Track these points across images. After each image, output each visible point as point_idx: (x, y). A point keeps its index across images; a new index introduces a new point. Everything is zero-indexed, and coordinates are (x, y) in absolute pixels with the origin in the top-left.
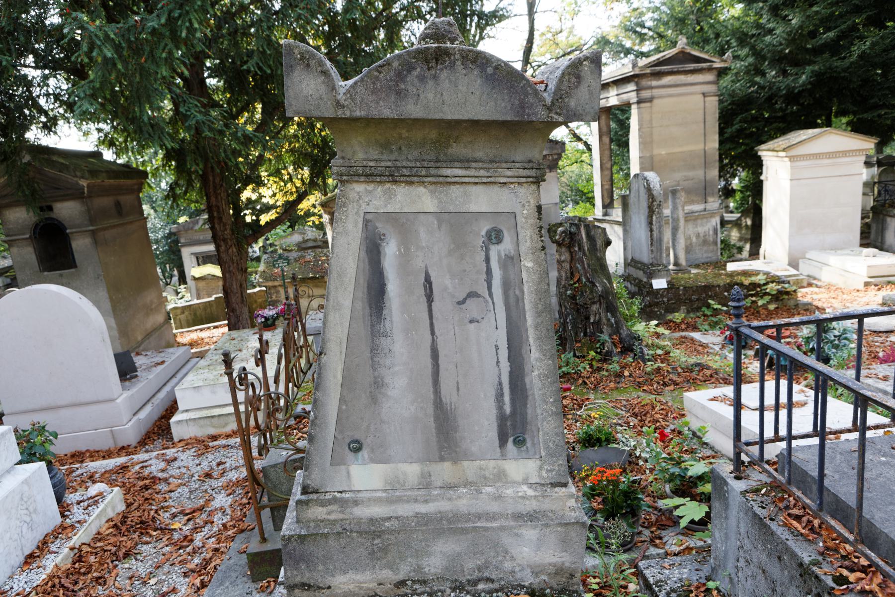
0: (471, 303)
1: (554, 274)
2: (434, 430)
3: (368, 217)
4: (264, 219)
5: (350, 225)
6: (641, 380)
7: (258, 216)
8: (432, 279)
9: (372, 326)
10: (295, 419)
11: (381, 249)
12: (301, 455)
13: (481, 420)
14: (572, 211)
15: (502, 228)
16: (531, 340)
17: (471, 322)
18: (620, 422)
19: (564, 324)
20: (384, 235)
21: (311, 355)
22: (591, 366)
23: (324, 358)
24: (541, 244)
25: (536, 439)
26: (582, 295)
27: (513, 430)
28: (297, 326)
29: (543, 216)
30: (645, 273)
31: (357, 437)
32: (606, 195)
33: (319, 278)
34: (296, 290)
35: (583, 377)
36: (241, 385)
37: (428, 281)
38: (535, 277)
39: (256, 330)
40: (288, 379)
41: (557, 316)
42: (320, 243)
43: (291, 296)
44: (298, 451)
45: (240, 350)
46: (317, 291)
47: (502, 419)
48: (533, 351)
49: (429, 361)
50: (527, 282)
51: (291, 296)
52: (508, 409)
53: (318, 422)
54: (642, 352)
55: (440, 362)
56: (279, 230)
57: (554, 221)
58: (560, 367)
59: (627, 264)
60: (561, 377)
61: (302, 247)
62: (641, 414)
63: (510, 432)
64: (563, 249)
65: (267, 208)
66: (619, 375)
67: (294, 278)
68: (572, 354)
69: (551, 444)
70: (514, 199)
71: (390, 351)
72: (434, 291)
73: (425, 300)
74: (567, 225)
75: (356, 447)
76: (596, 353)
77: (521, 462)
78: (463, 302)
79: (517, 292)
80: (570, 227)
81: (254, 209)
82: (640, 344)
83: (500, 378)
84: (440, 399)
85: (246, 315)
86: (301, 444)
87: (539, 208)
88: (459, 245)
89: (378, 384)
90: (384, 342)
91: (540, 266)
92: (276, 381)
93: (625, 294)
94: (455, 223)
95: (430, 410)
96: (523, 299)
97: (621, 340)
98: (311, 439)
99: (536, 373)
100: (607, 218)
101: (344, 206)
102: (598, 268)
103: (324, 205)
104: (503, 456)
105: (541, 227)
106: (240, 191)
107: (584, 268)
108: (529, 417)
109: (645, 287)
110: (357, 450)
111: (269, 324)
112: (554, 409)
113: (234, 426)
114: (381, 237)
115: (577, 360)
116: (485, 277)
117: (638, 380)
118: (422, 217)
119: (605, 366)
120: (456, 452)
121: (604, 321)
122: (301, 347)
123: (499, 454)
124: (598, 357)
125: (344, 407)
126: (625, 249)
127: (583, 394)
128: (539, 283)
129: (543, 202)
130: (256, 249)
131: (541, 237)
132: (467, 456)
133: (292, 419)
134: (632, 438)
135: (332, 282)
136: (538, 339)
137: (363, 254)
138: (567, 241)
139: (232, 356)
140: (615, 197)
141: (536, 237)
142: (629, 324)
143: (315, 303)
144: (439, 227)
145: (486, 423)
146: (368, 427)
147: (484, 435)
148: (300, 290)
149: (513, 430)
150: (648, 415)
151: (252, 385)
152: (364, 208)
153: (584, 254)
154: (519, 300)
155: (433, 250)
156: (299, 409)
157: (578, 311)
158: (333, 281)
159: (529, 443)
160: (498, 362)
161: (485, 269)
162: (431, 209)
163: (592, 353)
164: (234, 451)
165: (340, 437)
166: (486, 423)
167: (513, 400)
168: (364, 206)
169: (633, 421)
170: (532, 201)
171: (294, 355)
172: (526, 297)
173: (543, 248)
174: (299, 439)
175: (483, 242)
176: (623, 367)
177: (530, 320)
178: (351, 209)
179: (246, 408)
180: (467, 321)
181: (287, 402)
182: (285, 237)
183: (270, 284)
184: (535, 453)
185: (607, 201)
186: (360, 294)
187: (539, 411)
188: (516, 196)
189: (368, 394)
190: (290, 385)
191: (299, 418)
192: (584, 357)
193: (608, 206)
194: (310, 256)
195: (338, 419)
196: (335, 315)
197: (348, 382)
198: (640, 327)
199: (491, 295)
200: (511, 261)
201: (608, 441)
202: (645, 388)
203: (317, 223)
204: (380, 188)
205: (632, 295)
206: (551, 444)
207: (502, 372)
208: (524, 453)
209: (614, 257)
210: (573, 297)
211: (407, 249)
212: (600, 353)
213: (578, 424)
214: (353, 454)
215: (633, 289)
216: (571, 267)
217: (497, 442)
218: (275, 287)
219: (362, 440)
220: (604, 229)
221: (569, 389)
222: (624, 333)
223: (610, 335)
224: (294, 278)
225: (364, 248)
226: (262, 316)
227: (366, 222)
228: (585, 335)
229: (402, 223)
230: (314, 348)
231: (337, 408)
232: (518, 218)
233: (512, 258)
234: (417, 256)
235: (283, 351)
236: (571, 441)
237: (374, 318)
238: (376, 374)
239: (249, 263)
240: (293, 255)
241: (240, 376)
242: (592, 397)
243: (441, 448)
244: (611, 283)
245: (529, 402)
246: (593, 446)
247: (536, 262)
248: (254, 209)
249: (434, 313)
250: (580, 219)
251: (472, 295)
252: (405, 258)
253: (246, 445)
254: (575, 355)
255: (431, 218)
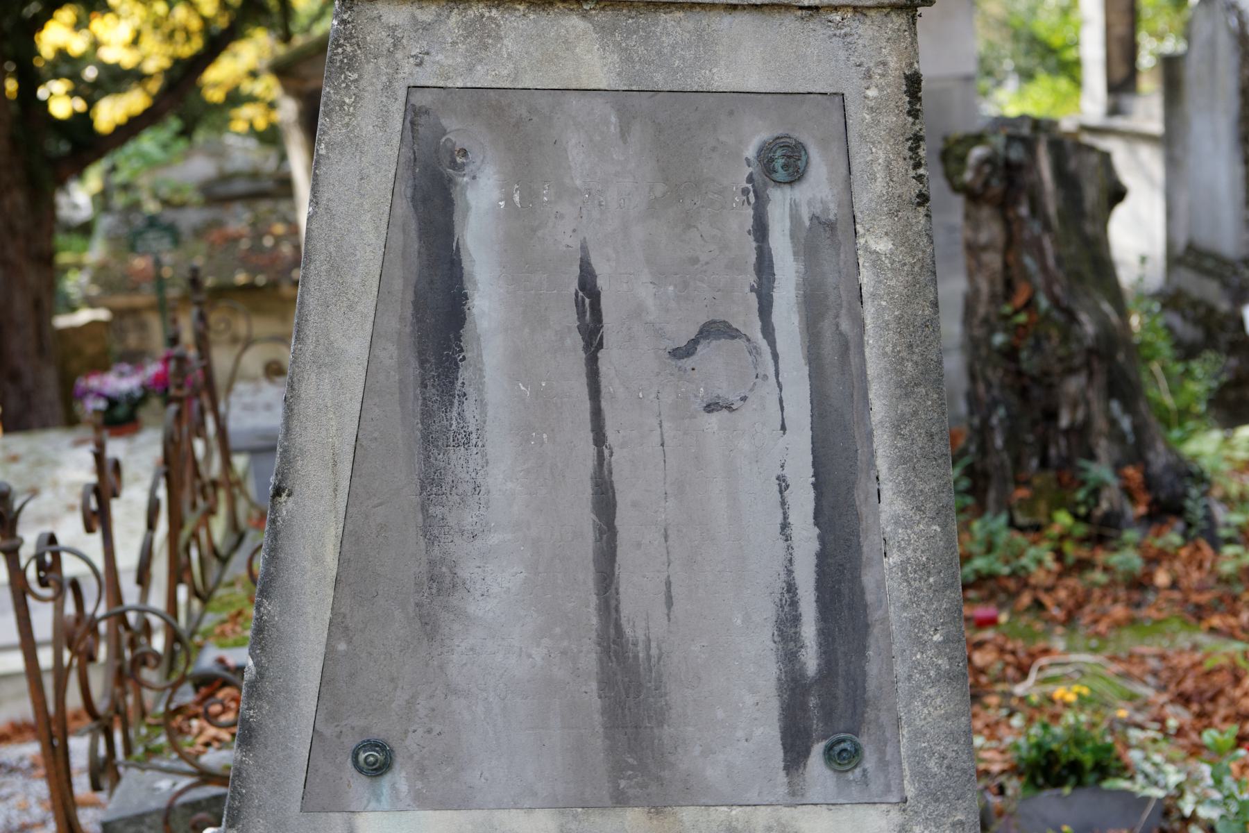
0: (711, 355)
1: (953, 287)
2: (597, 718)
3: (420, 99)
4: (110, 113)
5: (366, 124)
6: (1204, 598)
7: (91, 103)
8: (601, 283)
9: (427, 414)
10: (197, 688)
11: (455, 193)
12: (212, 790)
13: (733, 691)
14: (1011, 101)
15: (804, 138)
16: (882, 465)
17: (710, 408)
18: (1139, 718)
19: (982, 433)
20: (464, 153)
21: (242, 507)
22: (1059, 555)
23: (287, 505)
24: (915, 187)
25: (889, 750)
26: (1037, 348)
27: (824, 721)
28: (203, 424)
29: (926, 105)
30: (1225, 285)
31: (378, 731)
32: (1117, 52)
33: (268, 290)
34: (202, 317)
35: (1035, 588)
36: (43, 583)
37: (588, 288)
38: (896, 283)
39: (85, 432)
40: (178, 573)
41: (962, 407)
42: (268, 185)
43: (187, 336)
44: (206, 776)
45: (427, 53)
46: (263, 326)
47: (794, 691)
48: (887, 494)
49: (586, 519)
50: (874, 296)
51: (187, 336)
52: (811, 661)
53: (268, 687)
54: (1209, 518)
55: (618, 522)
56: (148, 142)
57: (960, 128)
58: (966, 558)
59: (1174, 260)
60: (966, 586)
61: (217, 194)
62: (1200, 696)
63: (816, 725)
64: (986, 212)
65: (117, 79)
66: (1139, 584)
67: (195, 281)
68: (1003, 519)
69: (932, 764)
70: (842, 55)
71: (477, 488)
72: (606, 319)
73: (580, 343)
74: (998, 141)
75: (376, 761)
76: (1076, 517)
77: (845, 813)
78: (687, 351)
79: (845, 326)
80: (1007, 147)
81: (75, 77)
82: (1205, 494)
83: (790, 572)
84: (618, 627)
85: (51, 392)
86: (213, 759)
87: (913, 83)
88: (679, 188)
89: (440, 583)
90: (458, 462)
91: (912, 251)
92: (143, 577)
93: (1164, 347)
94: (669, 121)
95: (589, 659)
96: (861, 345)
97: (1149, 483)
98: (246, 736)
99: (894, 559)
100: (1119, 122)
101: (351, 68)
102: (1086, 268)
103: (283, 70)
104: (796, 796)
105: (917, 139)
106: (38, 23)
107: (1044, 268)
108: (872, 685)
109: (1223, 327)
110: (378, 769)
111: (120, 418)
112: (943, 663)
113: (23, 709)
114: (456, 159)
115: (1020, 539)
116: (752, 278)
117: (1195, 598)
118: (574, 101)
119: (1101, 556)
120: (659, 779)
121: (1100, 424)
122: (215, 484)
123: (782, 790)
124: (1081, 530)
125: (342, 647)
126: (1170, 214)
127: (1031, 636)
128: (909, 300)
129: (927, 69)
130: (78, 198)
131: (917, 165)
132: (691, 792)
133: (187, 688)
134: (1170, 760)
135: (312, 285)
136: (903, 460)
137: (404, 207)
138: (997, 185)
139: (17, 505)
140: (1146, 60)
141: (902, 167)
142: (1176, 434)
143: (253, 360)
144: (624, 133)
145: (749, 700)
146: (411, 703)
147: (740, 734)
148: (213, 318)
149: (824, 721)
150: (1222, 701)
151: (75, 585)
152: (409, 73)
153: (1047, 226)
154: (850, 348)
155: (604, 198)
156: (207, 660)
157: (1023, 393)
158: (315, 291)
159: (870, 761)
160: (785, 526)
161: (753, 258)
162: (602, 80)
163: (1063, 519)
164: (17, 781)
165: (328, 731)
166: (749, 700)
167: (825, 635)
168: (407, 67)
169: (1176, 717)
170: (893, 62)
171: (194, 506)
172: (870, 339)
173: (923, 199)
174: (207, 745)
175: (750, 179)
176: (1155, 559)
177: (879, 406)
178: (372, 75)
179: (58, 657)
180: (698, 405)
181: (174, 637)
182: (167, 164)
183: (122, 301)
184: (888, 789)
185: (1120, 72)
186: (392, 323)
187: (900, 669)
188: (848, 47)
189: (411, 608)
190: (182, 592)
191: (208, 684)
192: (1037, 528)
193: (1122, 84)
194: (238, 220)
195: (325, 680)
196: (317, 394)
197: (352, 578)
198: (1205, 445)
199: (768, 331)
200: (827, 235)
201: (1103, 770)
202: (1216, 621)
203: (261, 124)
204: (455, 17)
205: (1187, 352)
206: (932, 764)
207: (797, 554)
208: (855, 791)
209: (1137, 236)
210: (1010, 353)
211: (530, 196)
212: (1086, 519)
213: (1017, 721)
214: (364, 780)
215: (1190, 333)
216: (1006, 266)
217: (778, 756)
218: (134, 312)
219: (394, 744)
220: (1106, 157)
221: (991, 622)
222: (1158, 459)
223: (1117, 468)
224: (195, 281)
225: (405, 190)
226: (100, 395)
227: (414, 115)
228: (1044, 463)
229: (516, 117)
230: (251, 487)
231: (321, 649)
232: (851, 109)
233: (831, 226)
234: (559, 216)
235: (162, 493)
236: (996, 768)
237: (431, 391)
238: (436, 552)
239: (60, 239)
240: (190, 218)
241: (39, 558)
242: (1059, 644)
243: (618, 770)
244: (1123, 313)
245: (871, 640)
246: (1059, 783)
247: (901, 237)
248: (75, 77)
249: (604, 382)
250: (1038, 125)
251: (716, 330)
252: (522, 222)
253: (57, 764)
254: (1012, 524)
255: (600, 107)
